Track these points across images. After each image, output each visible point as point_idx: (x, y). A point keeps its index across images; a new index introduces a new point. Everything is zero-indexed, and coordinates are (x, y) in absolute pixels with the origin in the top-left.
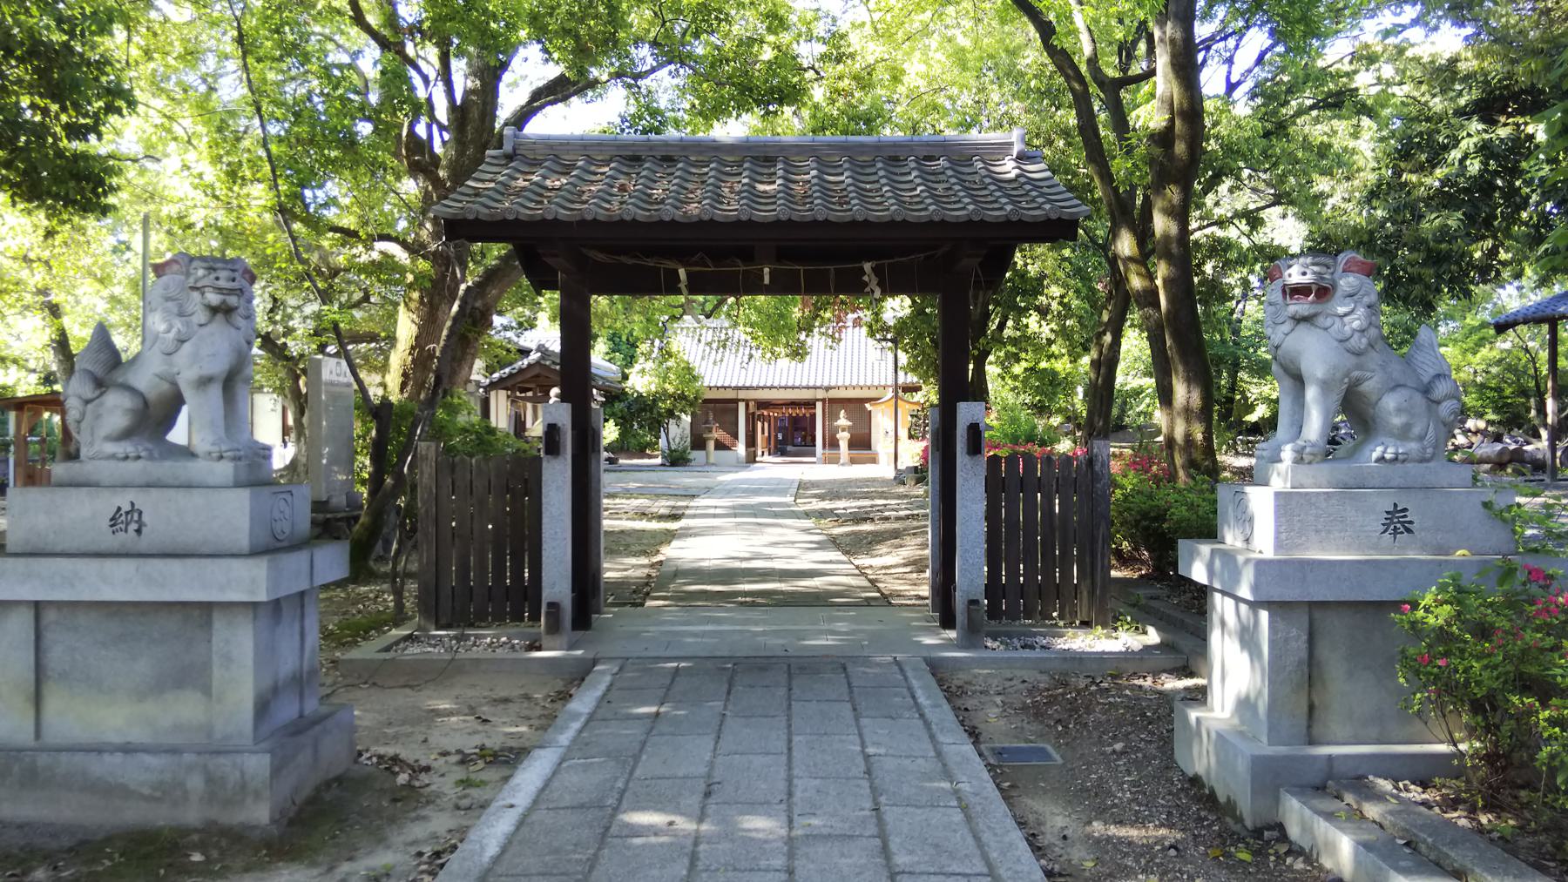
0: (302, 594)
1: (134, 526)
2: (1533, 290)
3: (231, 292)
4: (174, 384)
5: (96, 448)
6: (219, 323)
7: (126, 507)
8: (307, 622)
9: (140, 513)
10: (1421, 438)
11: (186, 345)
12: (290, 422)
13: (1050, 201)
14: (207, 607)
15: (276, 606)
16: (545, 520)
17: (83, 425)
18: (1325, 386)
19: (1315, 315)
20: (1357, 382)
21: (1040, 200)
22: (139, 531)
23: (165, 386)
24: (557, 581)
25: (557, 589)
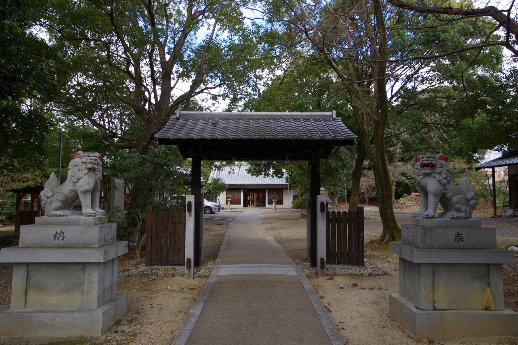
0: (113, 259)
1: (61, 238)
2: (447, 39)
3: (95, 164)
4: (77, 193)
5: (50, 213)
6: (91, 173)
7: (59, 232)
8: (114, 268)
9: (64, 234)
10: (465, 211)
11: (81, 180)
12: (103, 195)
13: (345, 134)
14: (84, 264)
15: (105, 263)
16: (186, 232)
17: (46, 206)
18: (436, 195)
19: (431, 173)
20: (445, 193)
21: (342, 133)
22: (63, 239)
23: (73, 193)
24: (189, 252)
25: (190, 254)
